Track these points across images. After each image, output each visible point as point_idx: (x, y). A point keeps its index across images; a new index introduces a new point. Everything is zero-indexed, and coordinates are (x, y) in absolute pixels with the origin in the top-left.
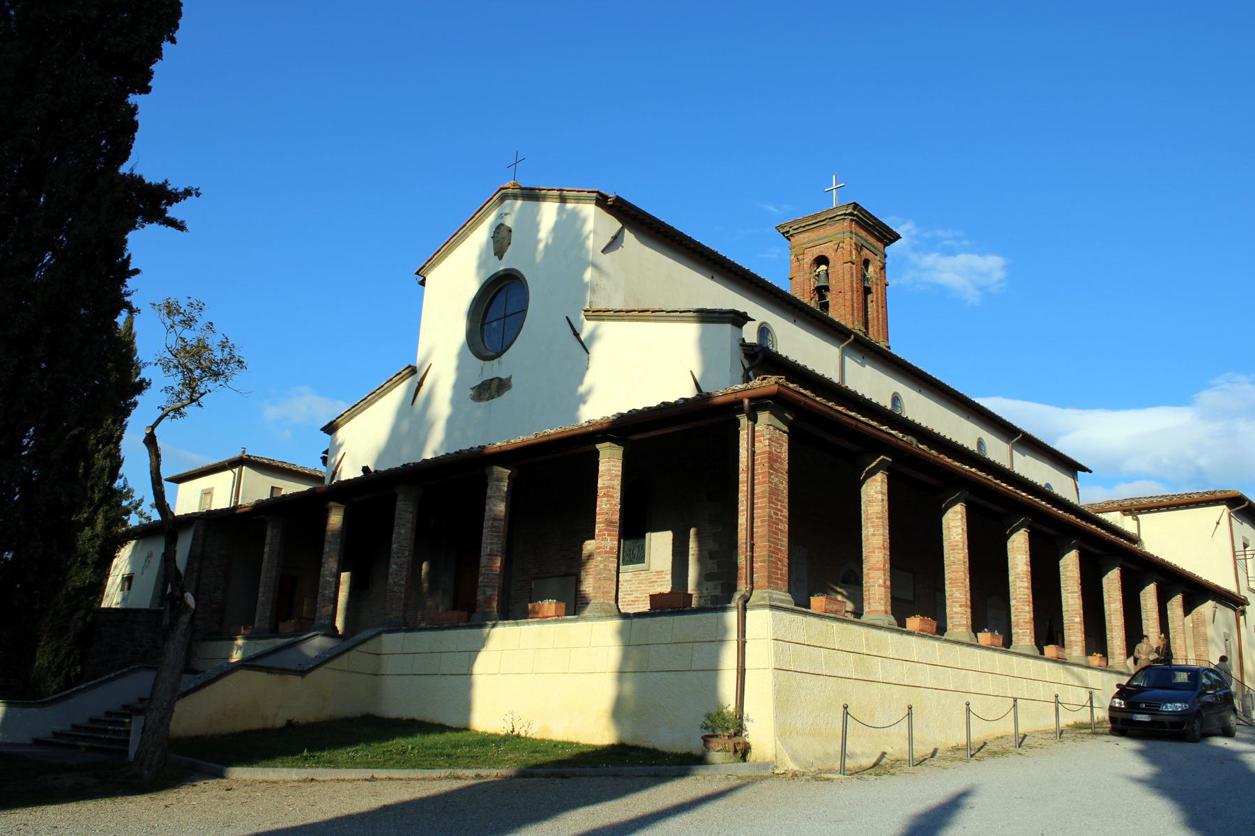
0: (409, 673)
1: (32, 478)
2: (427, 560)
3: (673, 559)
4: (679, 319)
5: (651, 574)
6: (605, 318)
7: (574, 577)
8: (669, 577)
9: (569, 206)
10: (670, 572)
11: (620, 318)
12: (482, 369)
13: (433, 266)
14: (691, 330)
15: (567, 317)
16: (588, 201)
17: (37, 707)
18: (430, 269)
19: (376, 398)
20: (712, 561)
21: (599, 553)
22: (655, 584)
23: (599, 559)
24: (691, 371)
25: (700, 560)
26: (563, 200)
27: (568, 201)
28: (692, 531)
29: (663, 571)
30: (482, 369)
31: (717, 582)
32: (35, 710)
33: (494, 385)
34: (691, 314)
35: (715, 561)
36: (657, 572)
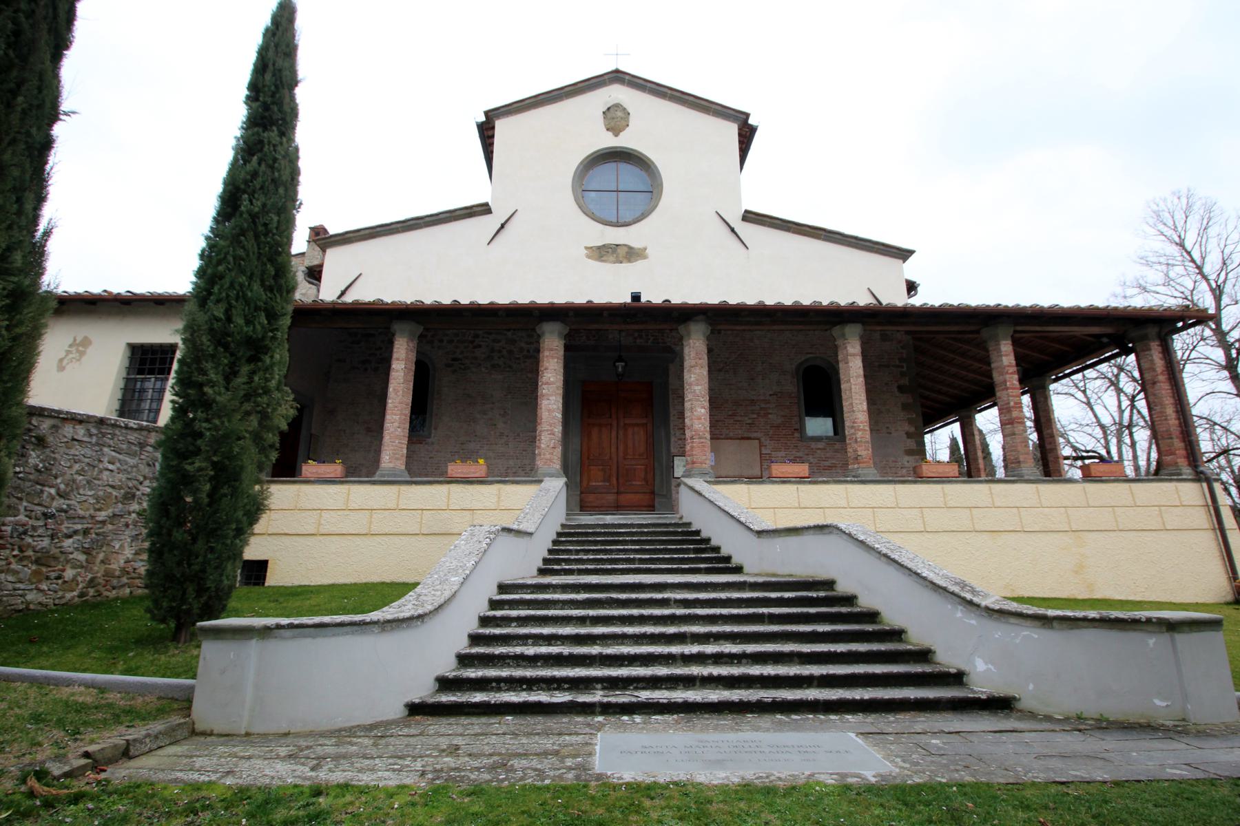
7: (757, 441)
20: (909, 440)
33: (622, 251)
35: (913, 440)
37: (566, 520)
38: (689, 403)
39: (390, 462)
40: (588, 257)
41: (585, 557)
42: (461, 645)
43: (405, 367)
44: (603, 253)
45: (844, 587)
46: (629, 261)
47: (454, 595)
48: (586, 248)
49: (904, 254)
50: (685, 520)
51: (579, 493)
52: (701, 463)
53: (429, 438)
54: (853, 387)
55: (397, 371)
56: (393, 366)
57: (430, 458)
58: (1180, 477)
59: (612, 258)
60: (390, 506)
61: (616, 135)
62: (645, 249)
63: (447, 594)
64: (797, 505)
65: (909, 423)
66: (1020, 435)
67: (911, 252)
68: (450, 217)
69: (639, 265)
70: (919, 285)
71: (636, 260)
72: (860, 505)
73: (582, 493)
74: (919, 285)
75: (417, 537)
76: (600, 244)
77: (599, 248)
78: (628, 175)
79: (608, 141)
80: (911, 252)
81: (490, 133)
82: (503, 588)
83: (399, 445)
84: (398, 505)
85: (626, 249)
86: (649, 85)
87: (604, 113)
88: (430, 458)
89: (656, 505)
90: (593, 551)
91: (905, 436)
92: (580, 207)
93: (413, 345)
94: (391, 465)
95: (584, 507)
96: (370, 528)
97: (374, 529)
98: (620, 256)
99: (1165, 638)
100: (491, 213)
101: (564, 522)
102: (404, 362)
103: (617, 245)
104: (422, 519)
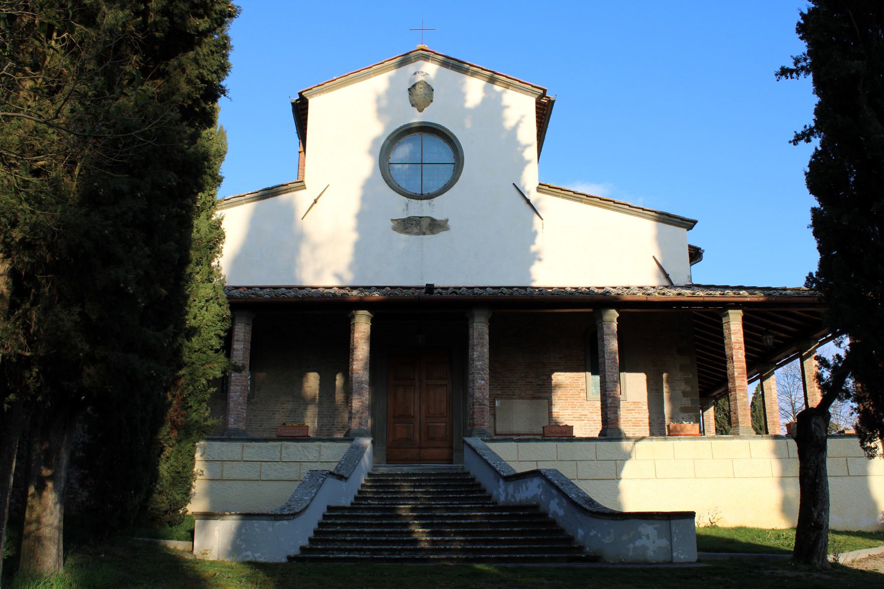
0: (218, 478)
1: (838, 366)
2: (338, 373)
3: (648, 394)
4: (640, 214)
5: (629, 404)
6: (561, 195)
8: (646, 407)
9: (497, 88)
10: (647, 403)
11: (579, 199)
12: (407, 205)
13: (322, 92)
14: (648, 227)
15: (514, 184)
16: (530, 93)
17: (287, 520)
18: (316, 94)
19: (244, 201)
20: (685, 399)
21: (741, 390)
22: (632, 411)
23: (742, 394)
24: (654, 257)
25: (672, 399)
26: (492, 80)
27: (497, 83)
28: (665, 375)
29: (640, 403)
30: (407, 205)
31: (692, 414)
32: (285, 522)
33: (425, 224)
34: (653, 214)
35: (689, 398)
36: (634, 403)
37: (372, 470)
38: (472, 376)
39: (235, 424)
40: (395, 229)
41: (385, 496)
42: (319, 518)
43: (244, 347)
44: (407, 225)
45: (477, 480)
46: (432, 233)
47: (307, 507)
48: (392, 220)
49: (689, 224)
50: (466, 470)
51: (385, 448)
52: (480, 425)
53: (253, 398)
54: (606, 361)
55: (238, 350)
56: (235, 346)
57: (254, 416)
58: (606, 437)
59: (416, 230)
60: (236, 458)
61: (421, 110)
62: (447, 220)
63: (304, 505)
64: (555, 459)
65: (685, 384)
66: (740, 399)
67: (695, 222)
68: (268, 194)
69: (442, 236)
70: (704, 251)
71: (439, 232)
72: (605, 459)
73: (387, 448)
74: (704, 251)
75: (257, 482)
76: (405, 217)
77: (404, 220)
78: (437, 150)
79: (416, 118)
80: (695, 222)
81: (305, 106)
82: (330, 508)
83: (241, 410)
84: (242, 458)
85: (428, 221)
86: (452, 61)
87: (409, 90)
88: (254, 416)
89: (454, 459)
90: (391, 492)
91: (681, 394)
92: (386, 182)
93: (249, 328)
94: (235, 426)
95: (390, 460)
96: (222, 475)
97: (225, 477)
98: (424, 227)
99: (665, 523)
100: (305, 188)
101: (371, 471)
102: (242, 343)
103: (421, 217)
104: (261, 468)
